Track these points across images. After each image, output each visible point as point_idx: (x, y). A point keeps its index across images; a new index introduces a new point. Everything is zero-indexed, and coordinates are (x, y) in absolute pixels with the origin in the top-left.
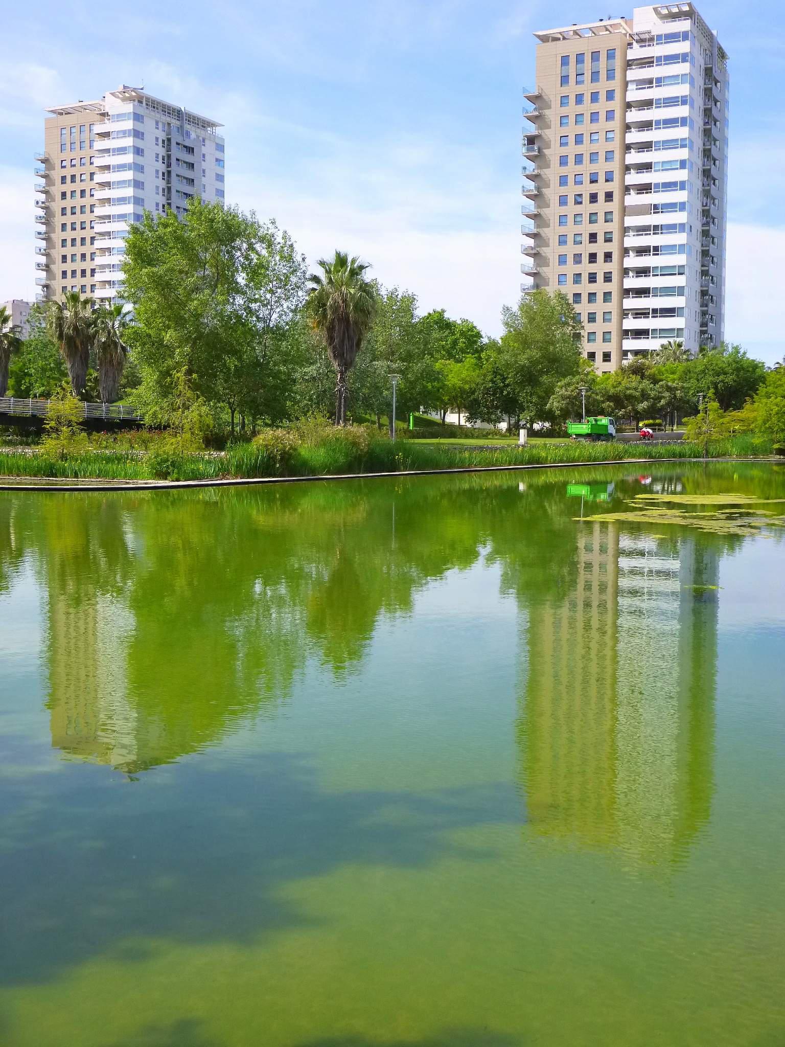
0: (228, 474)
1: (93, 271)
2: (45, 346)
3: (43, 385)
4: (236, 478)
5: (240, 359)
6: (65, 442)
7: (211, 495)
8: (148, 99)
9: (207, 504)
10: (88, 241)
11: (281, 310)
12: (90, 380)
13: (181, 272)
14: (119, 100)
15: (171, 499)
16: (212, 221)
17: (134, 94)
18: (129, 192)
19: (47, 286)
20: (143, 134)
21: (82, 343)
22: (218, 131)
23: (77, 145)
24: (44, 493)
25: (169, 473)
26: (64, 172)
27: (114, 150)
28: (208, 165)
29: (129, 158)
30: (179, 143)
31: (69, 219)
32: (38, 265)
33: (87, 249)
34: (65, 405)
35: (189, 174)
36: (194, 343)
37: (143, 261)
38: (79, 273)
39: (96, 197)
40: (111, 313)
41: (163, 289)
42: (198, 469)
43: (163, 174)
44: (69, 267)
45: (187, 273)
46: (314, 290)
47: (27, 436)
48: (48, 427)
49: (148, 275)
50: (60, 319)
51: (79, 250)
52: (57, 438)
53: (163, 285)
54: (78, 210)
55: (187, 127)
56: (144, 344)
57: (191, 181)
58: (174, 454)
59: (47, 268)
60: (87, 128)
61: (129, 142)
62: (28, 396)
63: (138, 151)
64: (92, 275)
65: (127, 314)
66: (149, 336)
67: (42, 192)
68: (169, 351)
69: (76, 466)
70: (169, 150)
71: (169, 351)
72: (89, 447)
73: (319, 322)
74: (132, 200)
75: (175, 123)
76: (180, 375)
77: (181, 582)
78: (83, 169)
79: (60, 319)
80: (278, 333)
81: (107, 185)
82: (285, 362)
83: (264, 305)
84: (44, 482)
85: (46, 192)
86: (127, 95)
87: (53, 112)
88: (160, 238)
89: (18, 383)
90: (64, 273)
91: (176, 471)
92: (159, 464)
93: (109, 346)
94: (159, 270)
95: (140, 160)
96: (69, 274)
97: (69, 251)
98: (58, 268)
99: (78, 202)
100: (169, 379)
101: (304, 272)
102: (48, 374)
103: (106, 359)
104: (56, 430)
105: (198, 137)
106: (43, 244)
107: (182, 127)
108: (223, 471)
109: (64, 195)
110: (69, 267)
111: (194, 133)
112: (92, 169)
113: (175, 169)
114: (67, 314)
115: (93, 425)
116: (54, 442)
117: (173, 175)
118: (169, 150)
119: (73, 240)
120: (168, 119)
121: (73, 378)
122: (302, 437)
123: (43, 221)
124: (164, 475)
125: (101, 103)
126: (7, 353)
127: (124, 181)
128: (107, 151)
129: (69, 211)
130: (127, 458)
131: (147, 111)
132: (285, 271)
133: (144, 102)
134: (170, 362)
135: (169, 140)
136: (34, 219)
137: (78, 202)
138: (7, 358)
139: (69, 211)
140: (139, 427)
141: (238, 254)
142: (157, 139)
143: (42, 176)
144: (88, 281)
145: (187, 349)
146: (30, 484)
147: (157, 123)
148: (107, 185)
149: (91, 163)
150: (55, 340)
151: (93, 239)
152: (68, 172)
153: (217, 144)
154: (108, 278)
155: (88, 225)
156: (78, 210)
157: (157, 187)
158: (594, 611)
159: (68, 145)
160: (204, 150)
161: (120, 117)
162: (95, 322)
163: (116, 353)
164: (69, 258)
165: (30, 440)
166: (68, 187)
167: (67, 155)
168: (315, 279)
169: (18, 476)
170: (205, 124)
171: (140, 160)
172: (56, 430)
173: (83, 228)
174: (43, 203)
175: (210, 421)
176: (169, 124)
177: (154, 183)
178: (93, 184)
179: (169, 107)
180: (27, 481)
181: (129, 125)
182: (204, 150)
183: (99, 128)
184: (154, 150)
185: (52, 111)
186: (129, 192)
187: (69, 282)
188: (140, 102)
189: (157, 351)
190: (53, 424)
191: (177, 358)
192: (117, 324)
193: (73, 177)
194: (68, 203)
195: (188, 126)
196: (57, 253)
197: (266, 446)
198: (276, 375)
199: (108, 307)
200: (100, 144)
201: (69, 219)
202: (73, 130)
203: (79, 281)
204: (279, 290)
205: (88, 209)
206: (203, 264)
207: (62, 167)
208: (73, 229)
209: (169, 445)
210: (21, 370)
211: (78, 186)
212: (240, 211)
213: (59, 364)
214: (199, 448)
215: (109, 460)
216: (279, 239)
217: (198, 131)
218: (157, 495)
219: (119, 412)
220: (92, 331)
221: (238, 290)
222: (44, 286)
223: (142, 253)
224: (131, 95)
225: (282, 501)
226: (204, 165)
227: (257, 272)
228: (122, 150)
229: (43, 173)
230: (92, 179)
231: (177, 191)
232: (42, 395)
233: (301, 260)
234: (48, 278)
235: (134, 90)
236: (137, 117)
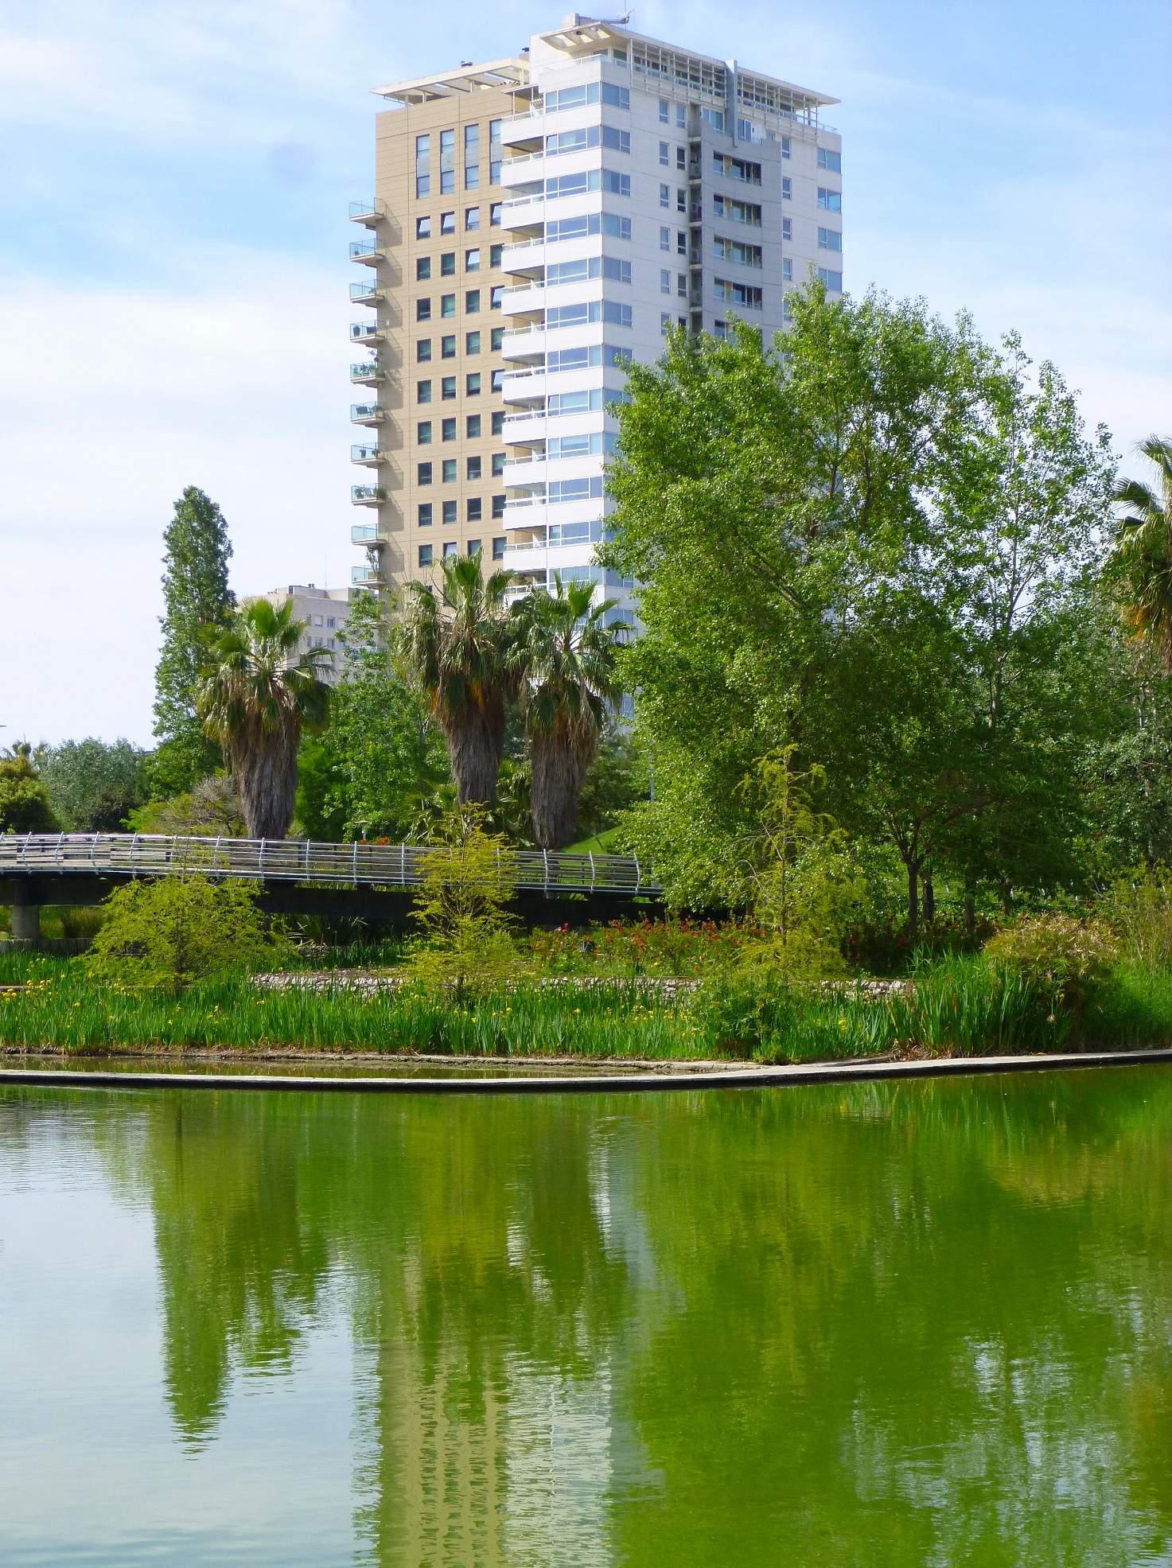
0: (917, 1043)
1: (499, 503)
2: (384, 703)
3: (378, 806)
4: (942, 1054)
5: (929, 720)
6: (467, 957)
7: (870, 1103)
8: (639, 47)
9: (854, 1125)
10: (486, 424)
11: (1036, 579)
12: (505, 788)
13: (769, 487)
14: (566, 55)
15: (762, 1112)
16: (856, 346)
17: (603, 35)
18: (592, 290)
19: (380, 547)
20: (627, 136)
21: (487, 692)
22: (824, 117)
23: (458, 177)
24: (416, 1096)
25: (756, 1042)
26: (423, 249)
27: (552, 183)
28: (800, 208)
29: (591, 203)
30: (721, 154)
31: (436, 370)
32: (359, 492)
33: (484, 446)
34: (471, 859)
35: (748, 234)
36: (807, 682)
37: (668, 464)
38: (462, 510)
39: (506, 309)
40: (561, 609)
41: (722, 538)
42: (835, 1030)
43: (681, 237)
44: (436, 493)
45: (786, 489)
46: (1132, 523)
47: (344, 942)
48: (421, 915)
49: (685, 502)
50: (430, 629)
51: (462, 448)
52: (448, 947)
53: (719, 525)
54: (460, 345)
55: (742, 110)
56: (673, 687)
57: (754, 253)
58: (769, 987)
59: (382, 499)
60: (482, 132)
61: (591, 159)
62: (338, 836)
63: (615, 183)
64: (497, 514)
65: (601, 610)
66: (684, 665)
67: (368, 303)
68: (741, 705)
69: (499, 1020)
70: (695, 174)
71: (741, 705)
72: (533, 970)
73: (1148, 614)
74: (600, 312)
75: (710, 102)
76: (773, 768)
77: (779, 1355)
78: (472, 239)
79: (430, 629)
80: (1037, 645)
81: (534, 275)
82: (1057, 728)
83: (996, 572)
84: (417, 1067)
85: (379, 303)
86: (585, 39)
87: (398, 96)
88: (713, 398)
89: (315, 802)
90: (425, 511)
91: (776, 1034)
92: (727, 1015)
93: (558, 697)
94: (715, 486)
95: (621, 205)
96: (437, 513)
97: (436, 451)
98: (408, 497)
99: (460, 323)
100: (747, 780)
101: (1108, 476)
102: (391, 774)
103: (548, 730)
104: (447, 925)
105: (771, 135)
106: (371, 437)
107: (728, 111)
108: (905, 1034)
109: (424, 307)
110: (436, 493)
111: (759, 124)
112: (497, 236)
113: (713, 223)
114: (448, 615)
115: (534, 911)
116: (436, 958)
117: (707, 239)
118: (695, 174)
119: (473, 421)
120: (693, 95)
121: (464, 784)
122: (1120, 930)
123: (372, 376)
124: (740, 1047)
125: (520, 64)
126: (293, 722)
127: (578, 265)
128: (536, 186)
129: (436, 349)
130: (632, 999)
131: (639, 78)
132: (1052, 475)
133: (630, 54)
134: (742, 735)
135: (695, 148)
136: (347, 375)
137: (460, 323)
138: (294, 735)
139: (436, 349)
140: (656, 911)
141: (925, 432)
142: (664, 147)
143: (369, 263)
144: (484, 529)
145: (791, 697)
146: (380, 1073)
147: (664, 106)
148: (534, 275)
149: (494, 222)
150: (415, 686)
151: (498, 418)
152: (434, 248)
153: (821, 151)
154: (556, 512)
155: (484, 384)
156: (460, 345)
157: (665, 274)
158: (442, 1525)
159: (459, 173)
160: (788, 168)
161: (570, 96)
162: (521, 636)
163: (577, 713)
164: (437, 472)
165: (351, 952)
166: (435, 287)
167: (432, 204)
168: (1136, 494)
169: (347, 1050)
170: (788, 100)
171: (621, 205)
172: (447, 925)
173: (472, 392)
174: (370, 330)
175: (856, 889)
176: (695, 107)
177: (657, 261)
178: (498, 276)
179: (695, 63)
180: (373, 1066)
181: (591, 115)
182: (788, 168)
183: (513, 130)
184: (656, 176)
185: (393, 95)
186: (592, 290)
187: (436, 534)
188: (620, 55)
189: (700, 705)
190: (435, 907)
191: (762, 721)
192: (576, 640)
193: (447, 260)
194: (434, 328)
195: (746, 110)
196: (406, 461)
197: (1024, 962)
198: (1029, 764)
199: (554, 594)
200: (516, 171)
201: (436, 370)
202: (449, 139)
203: (462, 530)
204: (1035, 529)
205: (485, 342)
206: (828, 466)
207: (420, 236)
208: (448, 394)
209: (755, 965)
210: (319, 765)
211: (459, 284)
212: (927, 318)
213: (419, 749)
214: (828, 971)
215: (587, 1003)
216: (1030, 388)
217: (772, 119)
218: (720, 1099)
219: (585, 874)
220: (512, 657)
221: (921, 533)
222: (372, 547)
223: (662, 441)
224: (597, 41)
225: (1073, 1123)
226: (788, 208)
227: (972, 479)
228: (573, 183)
229: (370, 254)
230: (495, 262)
231: (719, 282)
232: (374, 833)
233: (1096, 441)
234: (383, 526)
235: (604, 25)
236: (613, 95)
